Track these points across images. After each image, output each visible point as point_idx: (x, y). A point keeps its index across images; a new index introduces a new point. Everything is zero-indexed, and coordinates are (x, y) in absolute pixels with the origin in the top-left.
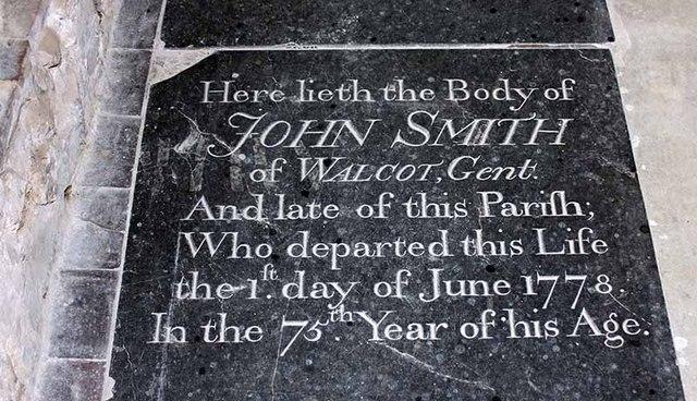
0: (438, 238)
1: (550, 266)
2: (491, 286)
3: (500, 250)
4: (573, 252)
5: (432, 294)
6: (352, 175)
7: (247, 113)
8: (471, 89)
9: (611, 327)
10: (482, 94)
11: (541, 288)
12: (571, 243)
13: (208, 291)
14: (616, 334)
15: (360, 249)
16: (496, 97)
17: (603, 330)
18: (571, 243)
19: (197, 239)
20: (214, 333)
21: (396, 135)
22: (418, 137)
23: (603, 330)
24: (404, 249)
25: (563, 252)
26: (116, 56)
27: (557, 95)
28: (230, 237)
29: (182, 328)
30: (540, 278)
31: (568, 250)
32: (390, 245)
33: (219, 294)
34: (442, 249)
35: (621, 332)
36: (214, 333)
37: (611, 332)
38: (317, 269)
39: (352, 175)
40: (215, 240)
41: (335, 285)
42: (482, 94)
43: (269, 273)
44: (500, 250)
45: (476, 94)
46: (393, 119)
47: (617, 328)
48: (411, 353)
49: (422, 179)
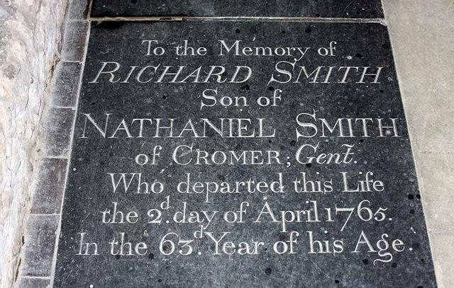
0: (276, 179)
9: (382, 245)
11: (341, 217)
12: (362, 182)
13: (193, 52)
14: (387, 251)
15: (224, 188)
17: (375, 248)
18: (362, 182)
20: (300, 186)
21: (271, 77)
22: (284, 77)
23: (375, 248)
24: (253, 187)
26: (72, 24)
27: (327, 52)
29: (138, 79)
30: (338, 210)
32: (244, 184)
33: (244, 52)
35: (390, 250)
36: (300, 186)
38: (196, 202)
40: (128, 178)
44: (317, 187)
46: (265, 67)
48: (176, 249)
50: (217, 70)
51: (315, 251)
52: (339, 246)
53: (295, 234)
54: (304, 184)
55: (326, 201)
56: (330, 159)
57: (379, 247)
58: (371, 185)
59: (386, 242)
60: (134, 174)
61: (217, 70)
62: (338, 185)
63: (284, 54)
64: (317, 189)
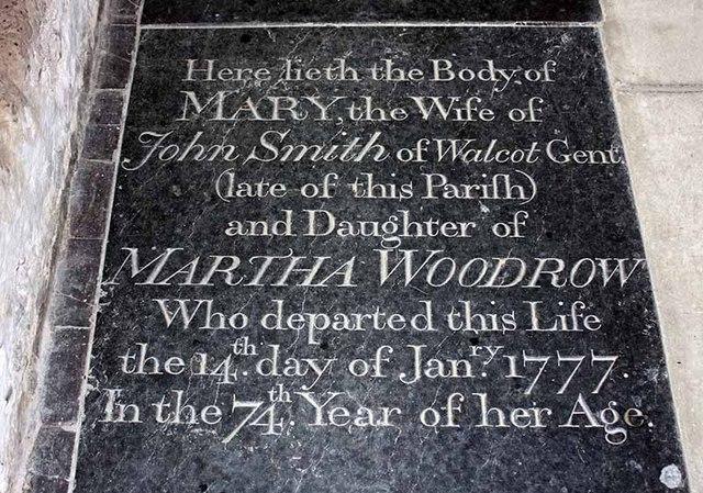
1: (538, 343)
2: (198, 412)
3: (492, 323)
4: (565, 328)
5: (413, 375)
6: (198, 276)
7: (108, 194)
8: (455, 69)
10: (466, 75)
12: (563, 318)
14: (394, 235)
16: (481, 78)
18: (563, 318)
19: (173, 307)
24: (382, 321)
25: (555, 329)
27: (411, 156)
28: (204, 306)
31: (560, 327)
34: (425, 323)
37: (606, 422)
39: (198, 276)
40: (190, 307)
41: (310, 361)
42: (466, 75)
43: (245, 346)
44: (492, 323)
45: (461, 75)
47: (616, 419)
49: (322, 259)
50: (226, 264)
51: (459, 373)
52: (536, 417)
53: (457, 398)
54: (466, 319)
55: (510, 343)
56: (289, 153)
57: (604, 421)
58: (580, 321)
59: (614, 412)
60: (201, 302)
61: (226, 264)
62: (524, 322)
63: (523, 117)
64: (490, 326)
